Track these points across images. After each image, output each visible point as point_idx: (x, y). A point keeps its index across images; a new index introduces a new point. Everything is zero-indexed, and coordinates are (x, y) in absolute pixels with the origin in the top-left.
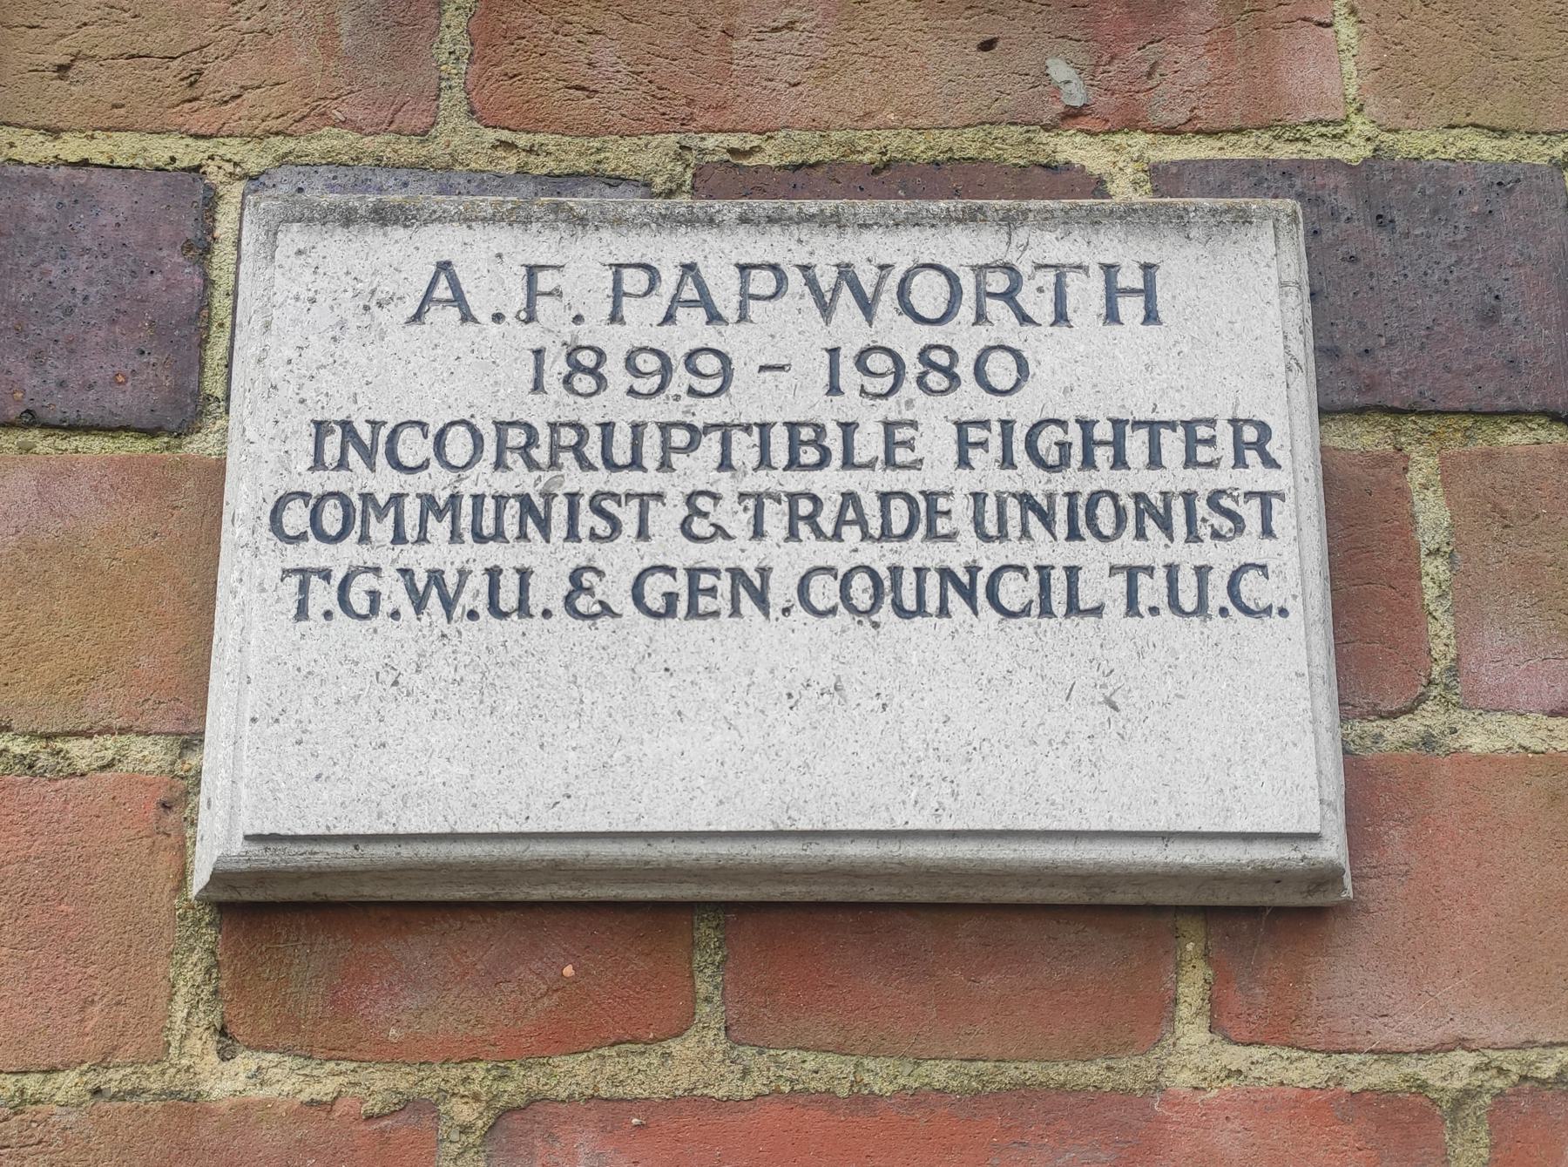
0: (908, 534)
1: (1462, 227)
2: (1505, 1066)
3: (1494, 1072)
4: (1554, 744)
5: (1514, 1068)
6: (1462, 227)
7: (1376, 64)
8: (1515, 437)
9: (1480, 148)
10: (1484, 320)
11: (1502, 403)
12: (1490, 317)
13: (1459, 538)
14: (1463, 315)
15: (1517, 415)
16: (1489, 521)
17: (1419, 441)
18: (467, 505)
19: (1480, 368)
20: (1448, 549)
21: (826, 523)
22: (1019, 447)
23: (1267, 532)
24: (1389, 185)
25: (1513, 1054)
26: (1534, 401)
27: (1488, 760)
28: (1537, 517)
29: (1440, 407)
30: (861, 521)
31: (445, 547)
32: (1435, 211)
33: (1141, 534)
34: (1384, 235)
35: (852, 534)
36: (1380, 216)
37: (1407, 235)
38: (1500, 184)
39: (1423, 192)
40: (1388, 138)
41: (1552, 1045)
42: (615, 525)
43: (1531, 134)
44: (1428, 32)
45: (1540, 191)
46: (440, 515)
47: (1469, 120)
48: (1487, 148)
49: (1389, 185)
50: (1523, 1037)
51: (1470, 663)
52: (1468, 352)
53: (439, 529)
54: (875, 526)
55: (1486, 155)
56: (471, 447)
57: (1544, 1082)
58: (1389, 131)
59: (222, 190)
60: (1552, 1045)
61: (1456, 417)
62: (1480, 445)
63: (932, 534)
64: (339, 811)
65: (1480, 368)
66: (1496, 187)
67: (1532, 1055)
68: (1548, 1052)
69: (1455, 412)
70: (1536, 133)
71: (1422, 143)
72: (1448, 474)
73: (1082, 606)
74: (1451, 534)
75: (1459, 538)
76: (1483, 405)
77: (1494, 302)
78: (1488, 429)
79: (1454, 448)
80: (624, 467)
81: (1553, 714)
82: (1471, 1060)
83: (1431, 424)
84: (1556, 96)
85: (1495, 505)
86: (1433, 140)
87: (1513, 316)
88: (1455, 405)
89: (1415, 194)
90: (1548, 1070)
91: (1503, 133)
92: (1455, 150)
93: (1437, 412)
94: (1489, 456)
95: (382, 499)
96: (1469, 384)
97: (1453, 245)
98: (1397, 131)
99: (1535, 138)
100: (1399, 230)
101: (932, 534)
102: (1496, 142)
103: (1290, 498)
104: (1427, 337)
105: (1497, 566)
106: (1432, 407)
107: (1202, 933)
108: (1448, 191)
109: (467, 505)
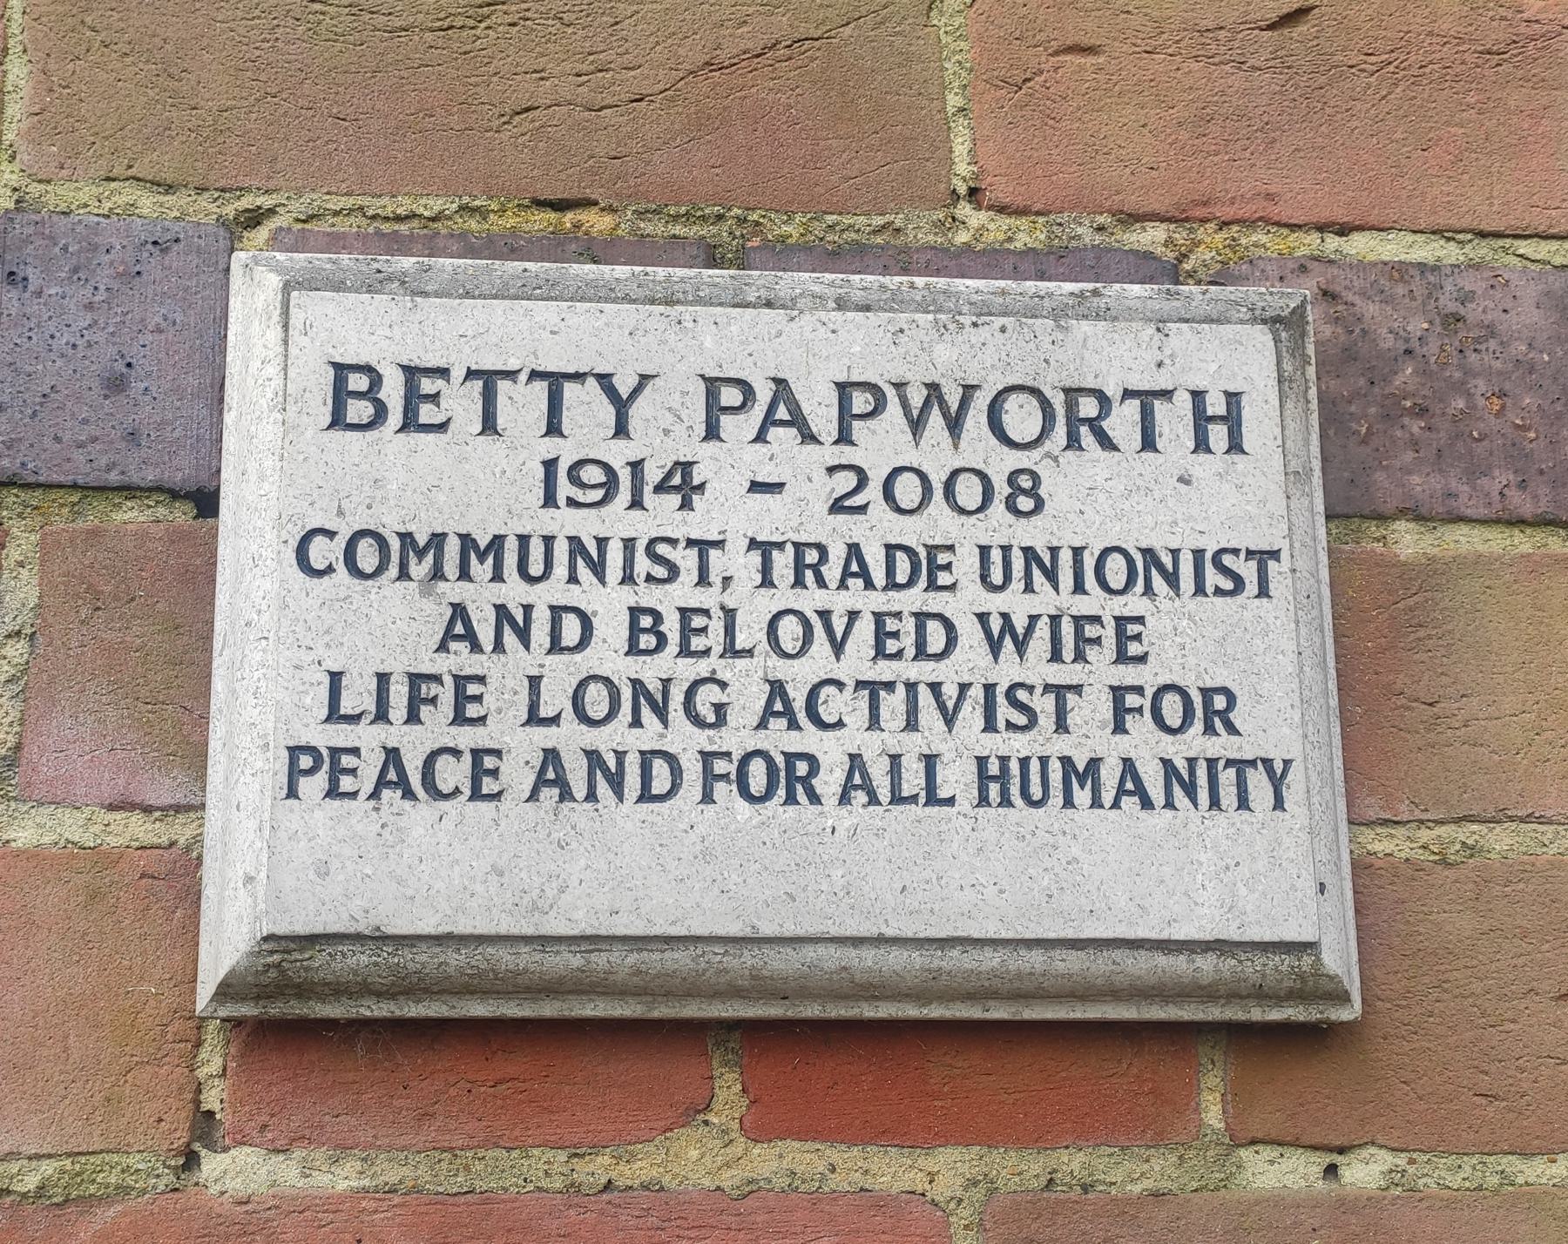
0: (910, 583)
1: (102, 287)
4: (108, 839)
6: (102, 287)
7: (36, 109)
8: (131, 514)
9: (139, 204)
10: (108, 388)
11: (114, 478)
12: (116, 385)
13: (44, 620)
14: (85, 383)
15: (129, 491)
16: (80, 602)
17: (20, 515)
18: (511, 546)
19: (94, 440)
20: (29, 631)
21: (832, 572)
23: (1263, 592)
24: (28, 241)
26: (150, 476)
27: (34, 855)
28: (133, 599)
29: (42, 479)
30: (864, 574)
31: (562, 585)
32: (76, 270)
33: (1029, 588)
34: (14, 294)
35: (856, 584)
36: (12, 274)
37: (39, 294)
38: (155, 243)
39: (65, 249)
40: (35, 189)
41: (38, 1157)
42: (674, 571)
43: (201, 190)
44: (103, 76)
45: (199, 251)
46: (482, 557)
47: (130, 172)
48: (147, 202)
49: (28, 241)
51: (31, 752)
52: (85, 421)
53: (481, 570)
54: (879, 577)
55: (145, 211)
56: (920, 489)
57: (24, 1195)
58: (40, 181)
60: (38, 1157)
61: (62, 491)
62: (91, 520)
63: (932, 586)
65: (94, 440)
66: (149, 246)
68: (34, 1163)
69: (61, 486)
70: (207, 189)
71: (78, 194)
72: (47, 549)
74: (37, 616)
75: (44, 620)
76: (91, 480)
77: (124, 370)
78: (99, 504)
79: (60, 523)
81: (112, 808)
83: (35, 498)
84: (235, 150)
85: (90, 586)
86: (87, 193)
87: (143, 385)
88: (56, 478)
89: (57, 250)
90: (30, 1183)
91: (170, 188)
92: (109, 205)
93: (39, 485)
94: (94, 533)
95: (422, 540)
96: (79, 457)
97: (90, 306)
98: (49, 182)
99: (206, 195)
100: (31, 288)
101: (932, 586)
102: (162, 198)
103: (1284, 555)
104: (41, 404)
105: (79, 651)
106: (32, 479)
107: (858, 976)
108: (94, 248)
109: (511, 546)
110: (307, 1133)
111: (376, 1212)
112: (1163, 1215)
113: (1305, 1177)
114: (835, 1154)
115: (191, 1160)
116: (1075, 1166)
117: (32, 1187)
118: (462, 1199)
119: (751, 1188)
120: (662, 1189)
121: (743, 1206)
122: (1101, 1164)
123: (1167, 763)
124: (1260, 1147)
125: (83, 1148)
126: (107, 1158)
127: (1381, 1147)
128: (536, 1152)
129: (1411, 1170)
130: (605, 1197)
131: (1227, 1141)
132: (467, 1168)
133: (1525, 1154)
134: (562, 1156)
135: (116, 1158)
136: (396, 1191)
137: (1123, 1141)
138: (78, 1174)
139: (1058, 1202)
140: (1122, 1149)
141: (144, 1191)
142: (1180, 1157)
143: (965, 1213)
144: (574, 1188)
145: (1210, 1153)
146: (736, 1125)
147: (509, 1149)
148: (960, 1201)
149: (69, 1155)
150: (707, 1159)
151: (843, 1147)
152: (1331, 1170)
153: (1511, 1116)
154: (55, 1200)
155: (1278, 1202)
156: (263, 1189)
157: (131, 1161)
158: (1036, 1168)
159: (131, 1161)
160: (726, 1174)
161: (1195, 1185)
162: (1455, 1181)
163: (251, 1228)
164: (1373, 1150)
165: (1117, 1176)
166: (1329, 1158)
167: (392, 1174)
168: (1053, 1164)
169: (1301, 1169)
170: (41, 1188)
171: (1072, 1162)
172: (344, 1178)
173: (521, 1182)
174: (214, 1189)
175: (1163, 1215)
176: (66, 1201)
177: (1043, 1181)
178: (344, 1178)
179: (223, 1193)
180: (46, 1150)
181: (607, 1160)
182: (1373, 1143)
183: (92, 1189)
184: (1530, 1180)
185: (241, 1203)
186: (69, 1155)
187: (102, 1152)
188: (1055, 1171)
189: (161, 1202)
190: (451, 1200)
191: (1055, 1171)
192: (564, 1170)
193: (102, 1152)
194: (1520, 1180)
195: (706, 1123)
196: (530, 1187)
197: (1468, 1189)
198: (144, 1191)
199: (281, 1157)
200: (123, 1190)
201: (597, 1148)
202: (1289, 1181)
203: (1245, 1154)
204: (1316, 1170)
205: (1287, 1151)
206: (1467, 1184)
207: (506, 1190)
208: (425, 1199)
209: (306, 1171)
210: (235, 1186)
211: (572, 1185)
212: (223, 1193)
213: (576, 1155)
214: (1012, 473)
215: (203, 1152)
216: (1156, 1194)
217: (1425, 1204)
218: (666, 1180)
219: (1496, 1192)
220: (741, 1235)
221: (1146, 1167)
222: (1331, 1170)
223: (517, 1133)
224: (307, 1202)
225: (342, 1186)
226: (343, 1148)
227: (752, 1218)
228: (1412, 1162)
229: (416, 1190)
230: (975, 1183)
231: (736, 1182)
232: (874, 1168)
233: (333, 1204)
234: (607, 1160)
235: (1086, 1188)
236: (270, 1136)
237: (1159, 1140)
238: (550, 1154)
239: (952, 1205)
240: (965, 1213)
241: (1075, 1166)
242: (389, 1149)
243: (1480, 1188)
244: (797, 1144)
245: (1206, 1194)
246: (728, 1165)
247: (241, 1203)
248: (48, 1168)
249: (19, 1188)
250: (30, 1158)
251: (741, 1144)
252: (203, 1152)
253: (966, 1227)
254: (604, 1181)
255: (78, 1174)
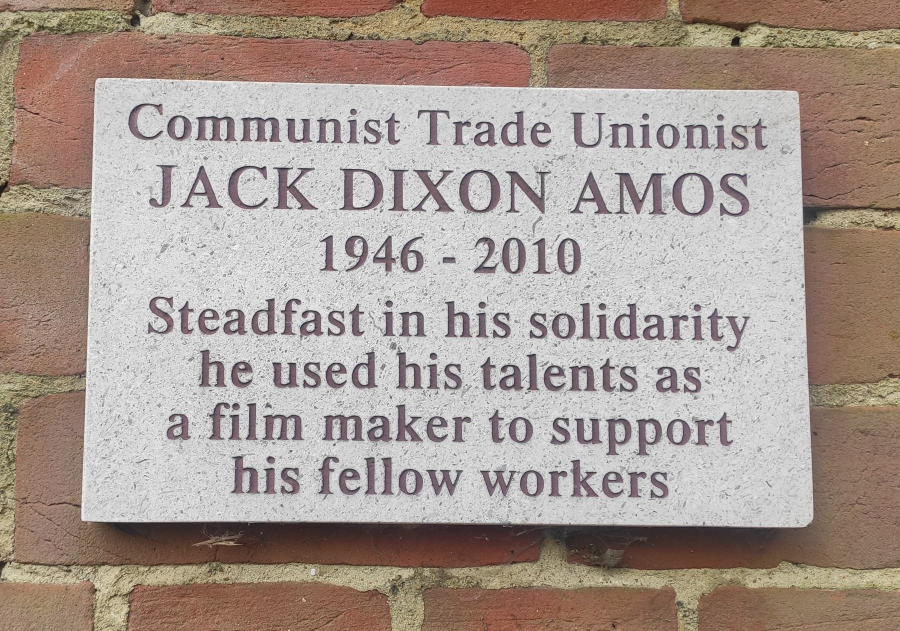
2: (30, 20)
3: (26, 24)
5: (35, 22)
22: (395, 482)
25: (37, 14)
50: (41, 5)
57: (51, 29)
59: (694, 605)
64: (473, 153)
67: (46, 15)
68: (56, 14)
73: (355, 205)
80: (253, 119)
82: (12, 17)
90: (54, 23)
110: (194, 5)
111: (230, 45)
112: (645, 56)
113: (721, 41)
114: (471, 23)
115: (135, 21)
116: (598, 31)
117: (55, 25)
118: (275, 41)
119: (426, 39)
120: (379, 39)
121: (421, 48)
122: (611, 30)
123: (625, 178)
124: (698, 25)
125: (80, 6)
126: (93, 12)
127: (764, 25)
128: (313, 18)
129: (779, 36)
130: (349, 42)
131: (681, 19)
132: (277, 25)
133: (841, 31)
134: (327, 22)
135: (97, 12)
136: (241, 35)
137: (625, 19)
138: (78, 19)
139: (588, 49)
140: (624, 22)
141: (112, 30)
142: (655, 28)
143: (539, 53)
144: (333, 37)
145: (672, 26)
146: (418, 9)
147: (299, 17)
148: (536, 47)
149: (73, 10)
150: (403, 25)
151: (475, 20)
152: (736, 41)
153: (835, 10)
154: (67, 32)
155: (706, 51)
156: (173, 32)
157: (105, 14)
158: (577, 32)
159: (105, 14)
160: (412, 32)
161: (662, 42)
162: (803, 43)
163: (167, 50)
164: (759, 27)
165: (621, 36)
166: (735, 33)
167: (238, 27)
168: (587, 29)
169: (720, 37)
170: (60, 25)
171: (597, 29)
172: (214, 28)
173: (305, 33)
174: (148, 32)
175: (645, 56)
176: (73, 33)
177: (581, 38)
178: (214, 28)
179: (152, 34)
180: (61, 6)
181: (350, 24)
182: (759, 23)
183: (86, 27)
184: (844, 44)
185: (161, 38)
186: (73, 10)
187: (89, 9)
188: (587, 33)
189: (121, 35)
190: (269, 41)
191: (587, 33)
192: (328, 27)
193: (89, 9)
194: (838, 44)
195: (403, 7)
196: (310, 36)
197: (809, 47)
198: (112, 30)
199: (181, 19)
200: (101, 29)
201: (345, 18)
202: (713, 43)
203: (689, 28)
204: (728, 39)
205: (714, 28)
206: (809, 44)
207: (298, 37)
208: (257, 40)
209: (195, 25)
210: (158, 30)
211: (332, 35)
212: (152, 34)
213: (334, 22)
214: (476, 136)
215: (141, 16)
216: (641, 46)
217: (785, 54)
218: (381, 35)
219: (824, 48)
220: (420, 62)
221: (636, 32)
222: (736, 41)
223: (303, 8)
224: (196, 39)
225: (213, 32)
226: (213, 14)
227: (426, 53)
228: (780, 32)
229: (251, 35)
230: (544, 39)
231: (418, 35)
232: (491, 30)
233: (208, 41)
234: (350, 24)
235: (604, 42)
236: (175, 6)
237: (644, 19)
238: (320, 20)
239: (532, 49)
240: (539, 53)
241: (598, 31)
242: (237, 14)
243: (815, 47)
244: (450, 18)
245: (667, 47)
246: (413, 27)
247: (161, 38)
248: (63, 15)
249: (49, 25)
250: (54, 11)
251: (420, 18)
252: (141, 16)
253: (539, 60)
254: (349, 33)
255: (78, 19)
